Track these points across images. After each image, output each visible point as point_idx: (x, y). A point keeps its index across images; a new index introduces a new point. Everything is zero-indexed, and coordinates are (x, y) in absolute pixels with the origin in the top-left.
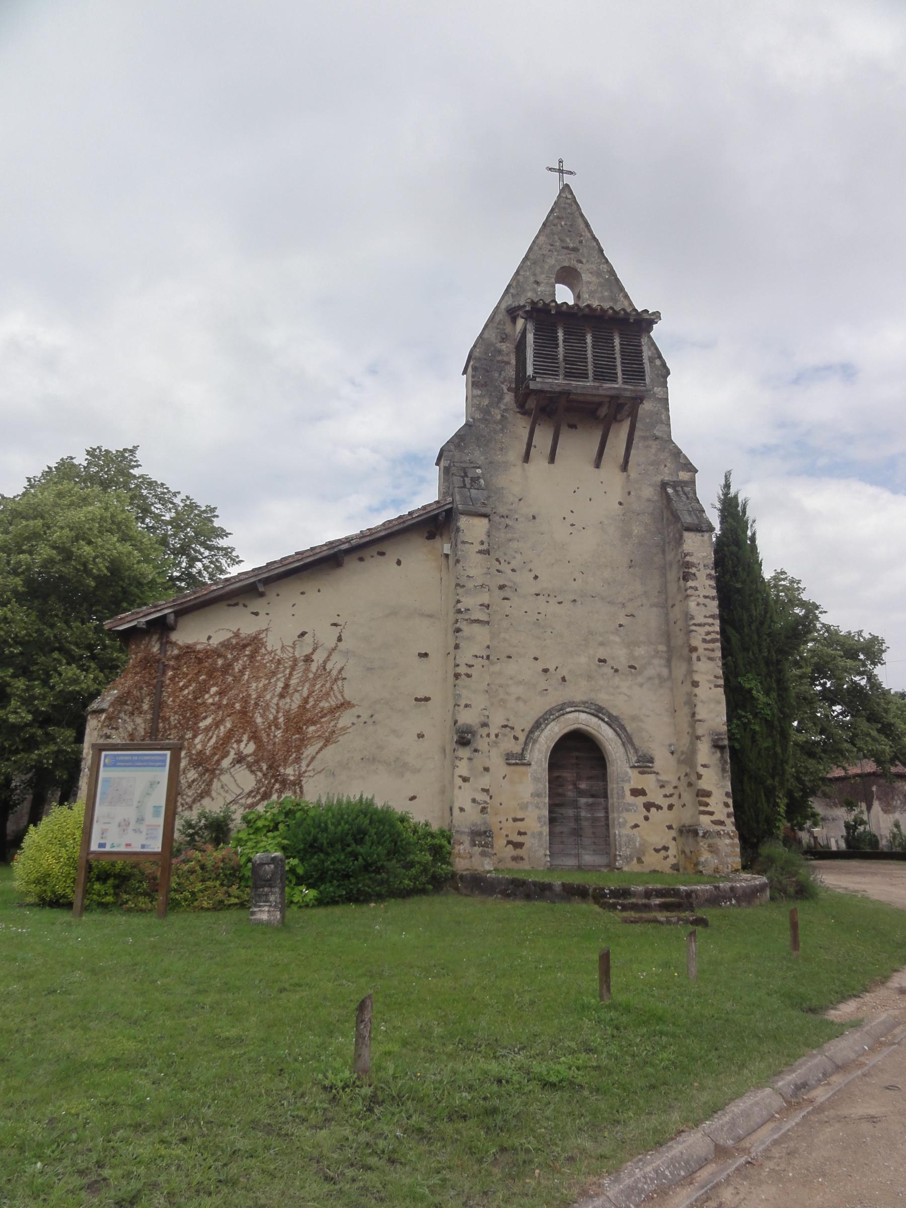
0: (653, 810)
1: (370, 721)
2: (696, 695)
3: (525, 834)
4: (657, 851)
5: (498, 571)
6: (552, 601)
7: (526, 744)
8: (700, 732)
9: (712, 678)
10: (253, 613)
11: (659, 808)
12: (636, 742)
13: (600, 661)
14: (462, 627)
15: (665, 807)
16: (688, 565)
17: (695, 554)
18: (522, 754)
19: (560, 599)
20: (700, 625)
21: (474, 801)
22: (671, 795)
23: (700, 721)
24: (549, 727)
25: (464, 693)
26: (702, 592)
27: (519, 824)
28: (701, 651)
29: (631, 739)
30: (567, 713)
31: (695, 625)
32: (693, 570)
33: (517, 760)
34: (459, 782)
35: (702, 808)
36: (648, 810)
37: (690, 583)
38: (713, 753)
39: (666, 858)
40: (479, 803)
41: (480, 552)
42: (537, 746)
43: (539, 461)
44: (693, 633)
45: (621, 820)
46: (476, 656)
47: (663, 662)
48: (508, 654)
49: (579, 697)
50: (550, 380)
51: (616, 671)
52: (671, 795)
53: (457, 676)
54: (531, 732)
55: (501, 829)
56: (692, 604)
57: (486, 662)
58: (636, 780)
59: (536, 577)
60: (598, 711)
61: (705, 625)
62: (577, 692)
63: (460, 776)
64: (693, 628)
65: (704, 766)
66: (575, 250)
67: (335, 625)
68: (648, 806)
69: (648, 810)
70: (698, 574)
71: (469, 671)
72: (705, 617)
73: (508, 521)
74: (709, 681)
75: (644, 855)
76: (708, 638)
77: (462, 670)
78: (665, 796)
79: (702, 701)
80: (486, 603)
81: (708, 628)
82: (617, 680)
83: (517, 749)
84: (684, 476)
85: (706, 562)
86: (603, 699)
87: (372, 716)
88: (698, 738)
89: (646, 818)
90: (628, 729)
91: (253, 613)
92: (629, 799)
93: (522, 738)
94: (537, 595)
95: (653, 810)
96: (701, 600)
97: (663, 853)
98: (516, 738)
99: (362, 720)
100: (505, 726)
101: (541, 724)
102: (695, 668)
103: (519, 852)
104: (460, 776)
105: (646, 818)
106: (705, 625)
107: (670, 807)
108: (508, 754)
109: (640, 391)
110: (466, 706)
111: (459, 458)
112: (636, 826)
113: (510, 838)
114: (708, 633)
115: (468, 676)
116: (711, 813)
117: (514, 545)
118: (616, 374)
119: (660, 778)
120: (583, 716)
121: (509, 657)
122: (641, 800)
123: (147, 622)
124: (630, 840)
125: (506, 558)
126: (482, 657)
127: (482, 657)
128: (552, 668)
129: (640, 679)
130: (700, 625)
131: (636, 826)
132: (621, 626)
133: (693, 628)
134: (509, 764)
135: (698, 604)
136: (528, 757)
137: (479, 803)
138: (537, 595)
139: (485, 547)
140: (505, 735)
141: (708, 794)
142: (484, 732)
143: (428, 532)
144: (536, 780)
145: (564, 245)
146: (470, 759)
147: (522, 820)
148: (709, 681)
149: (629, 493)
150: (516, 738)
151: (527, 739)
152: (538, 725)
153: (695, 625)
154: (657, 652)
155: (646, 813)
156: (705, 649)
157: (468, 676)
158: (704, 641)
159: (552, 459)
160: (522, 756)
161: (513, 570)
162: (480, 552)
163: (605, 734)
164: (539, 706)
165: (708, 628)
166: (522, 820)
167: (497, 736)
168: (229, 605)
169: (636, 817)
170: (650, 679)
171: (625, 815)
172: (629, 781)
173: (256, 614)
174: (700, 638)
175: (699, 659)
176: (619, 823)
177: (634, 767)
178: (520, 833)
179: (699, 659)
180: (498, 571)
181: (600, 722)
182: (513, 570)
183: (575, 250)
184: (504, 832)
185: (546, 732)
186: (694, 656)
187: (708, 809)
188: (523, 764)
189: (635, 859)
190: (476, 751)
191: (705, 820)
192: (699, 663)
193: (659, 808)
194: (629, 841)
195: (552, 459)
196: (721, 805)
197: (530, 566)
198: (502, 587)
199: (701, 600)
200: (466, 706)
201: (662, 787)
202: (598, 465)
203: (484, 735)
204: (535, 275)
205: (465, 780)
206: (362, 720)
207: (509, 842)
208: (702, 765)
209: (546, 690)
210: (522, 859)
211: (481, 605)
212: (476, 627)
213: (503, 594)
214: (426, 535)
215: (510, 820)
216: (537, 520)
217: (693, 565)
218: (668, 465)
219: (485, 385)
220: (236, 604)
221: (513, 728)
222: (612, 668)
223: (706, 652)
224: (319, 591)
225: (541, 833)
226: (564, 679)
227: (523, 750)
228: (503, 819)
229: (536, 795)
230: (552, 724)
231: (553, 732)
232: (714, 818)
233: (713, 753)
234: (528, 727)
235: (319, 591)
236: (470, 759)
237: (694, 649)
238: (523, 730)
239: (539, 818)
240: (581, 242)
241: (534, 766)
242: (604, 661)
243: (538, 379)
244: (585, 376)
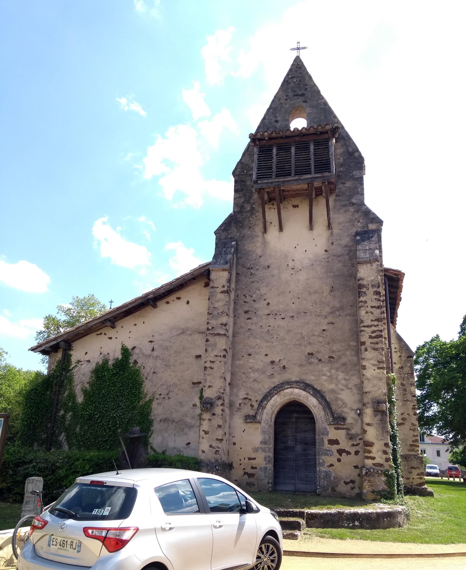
0: (344, 454)
1: (167, 397)
2: (363, 375)
3: (256, 468)
4: (346, 483)
5: (245, 302)
6: (278, 317)
7: (258, 409)
8: (366, 400)
9: (376, 362)
10: (109, 338)
11: (348, 453)
12: (334, 407)
13: (309, 354)
14: (209, 338)
15: (353, 453)
16: (361, 286)
17: (365, 279)
18: (255, 416)
19: (283, 316)
20: (367, 326)
21: (211, 446)
22: (357, 445)
23: (366, 393)
24: (273, 398)
25: (208, 378)
26: (370, 304)
27: (252, 461)
28: (368, 344)
29: (329, 405)
30: (286, 389)
31: (364, 326)
32: (364, 290)
33: (251, 419)
34: (202, 433)
35: (367, 454)
36: (341, 455)
37: (362, 299)
38: (375, 416)
39: (352, 488)
40: (214, 448)
41: (222, 292)
42: (265, 411)
43: (273, 232)
44: (363, 333)
45: (321, 461)
46: (217, 356)
47: (353, 353)
48: (249, 352)
49: (294, 379)
50: (266, 181)
51: (320, 360)
52: (357, 445)
53: (205, 368)
54: (262, 401)
55: (241, 464)
56: (363, 312)
57: (222, 359)
58: (333, 434)
59: (268, 304)
60: (306, 386)
61: (371, 326)
62: (293, 375)
63: (203, 431)
64: (363, 329)
65: (368, 424)
66: (303, 95)
67: (151, 342)
68: (340, 452)
69: (341, 455)
70: (367, 292)
71: (212, 365)
72: (372, 320)
73: (252, 271)
74: (374, 365)
75: (337, 486)
76: (373, 335)
77: (208, 365)
78: (353, 445)
79: (368, 379)
80: (224, 323)
81: (373, 328)
82: (320, 366)
83: (252, 413)
84: (372, 227)
85: (373, 283)
86: (310, 379)
87: (168, 394)
88: (364, 405)
89: (339, 460)
90: (327, 399)
91: (109, 338)
92: (327, 446)
93: (256, 406)
94: (269, 315)
95: (344, 454)
96: (369, 309)
97: (351, 485)
98: (252, 406)
99: (162, 396)
100: (246, 398)
101: (268, 397)
102: (363, 356)
103: (252, 480)
104: (203, 431)
105: (339, 460)
106: (371, 326)
107: (357, 453)
108: (246, 416)
109: (326, 176)
110: (210, 387)
111: (230, 236)
112: (331, 465)
113: (246, 471)
114: (373, 332)
115: (211, 368)
116: (373, 458)
117: (255, 285)
118: (310, 169)
119: (350, 432)
120: (297, 391)
121: (250, 355)
122: (335, 448)
123: (50, 347)
124: (328, 475)
125: (250, 293)
126: (221, 356)
127: (221, 356)
128: (277, 360)
129: (336, 365)
130: (367, 326)
131: (331, 465)
132: (324, 330)
133: (363, 329)
134: (247, 423)
135: (367, 313)
136: (258, 418)
137: (214, 448)
138: (269, 315)
139: (225, 289)
140: (245, 404)
141: (371, 444)
142: (220, 402)
143: (205, 283)
144: (264, 432)
145: (295, 94)
146: (210, 420)
147: (254, 459)
148: (374, 365)
149: (332, 243)
150: (252, 406)
151: (259, 406)
152: (267, 396)
153: (364, 326)
154: (349, 346)
155: (339, 457)
156: (371, 343)
157: (211, 368)
158: (371, 337)
159: (281, 229)
160: (254, 417)
161: (254, 301)
162: (222, 292)
163: (312, 402)
164: (267, 385)
165: (373, 328)
166: (254, 459)
167: (240, 404)
168: (97, 335)
169: (332, 459)
170: (344, 364)
171: (323, 457)
172: (327, 434)
173: (110, 338)
174: (367, 335)
175: (366, 350)
176: (320, 463)
177: (331, 424)
178: (253, 468)
179: (366, 350)
180: (245, 302)
181: (308, 394)
182: (254, 301)
183: (303, 95)
184: (242, 467)
185: (272, 401)
186: (363, 348)
187: (371, 455)
188: (256, 422)
189: (330, 488)
190: (214, 414)
191: (369, 462)
192: (367, 352)
193: (348, 453)
194: (326, 475)
195: (281, 229)
196: (380, 453)
197: (265, 297)
198: (246, 312)
199: (369, 309)
200: (210, 387)
201: (351, 438)
202: (311, 227)
203: (219, 405)
204: (275, 117)
205: (206, 433)
206: (162, 396)
207: (245, 473)
208: (367, 424)
209: (272, 375)
210: (253, 485)
211: (221, 324)
212: (217, 338)
213: (247, 316)
214: (204, 285)
215: (247, 459)
216: (270, 268)
217: (364, 286)
218: (361, 221)
219: (242, 190)
220: (101, 334)
221: (250, 400)
222: (318, 358)
223: (373, 345)
224: (144, 323)
225: (266, 468)
226: (284, 367)
227: (256, 413)
228: (242, 459)
229: (264, 442)
230: (276, 397)
231: (277, 401)
232: (374, 462)
233: (375, 416)
234: (260, 398)
235: (144, 323)
236: (210, 420)
237: (363, 343)
238: (257, 401)
239: (265, 458)
240: (306, 89)
241: (263, 424)
242: (312, 354)
243: (259, 182)
244: (289, 174)
